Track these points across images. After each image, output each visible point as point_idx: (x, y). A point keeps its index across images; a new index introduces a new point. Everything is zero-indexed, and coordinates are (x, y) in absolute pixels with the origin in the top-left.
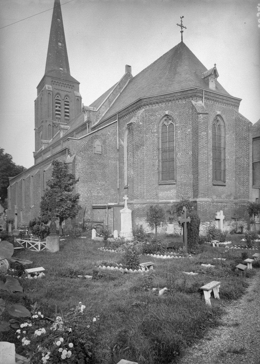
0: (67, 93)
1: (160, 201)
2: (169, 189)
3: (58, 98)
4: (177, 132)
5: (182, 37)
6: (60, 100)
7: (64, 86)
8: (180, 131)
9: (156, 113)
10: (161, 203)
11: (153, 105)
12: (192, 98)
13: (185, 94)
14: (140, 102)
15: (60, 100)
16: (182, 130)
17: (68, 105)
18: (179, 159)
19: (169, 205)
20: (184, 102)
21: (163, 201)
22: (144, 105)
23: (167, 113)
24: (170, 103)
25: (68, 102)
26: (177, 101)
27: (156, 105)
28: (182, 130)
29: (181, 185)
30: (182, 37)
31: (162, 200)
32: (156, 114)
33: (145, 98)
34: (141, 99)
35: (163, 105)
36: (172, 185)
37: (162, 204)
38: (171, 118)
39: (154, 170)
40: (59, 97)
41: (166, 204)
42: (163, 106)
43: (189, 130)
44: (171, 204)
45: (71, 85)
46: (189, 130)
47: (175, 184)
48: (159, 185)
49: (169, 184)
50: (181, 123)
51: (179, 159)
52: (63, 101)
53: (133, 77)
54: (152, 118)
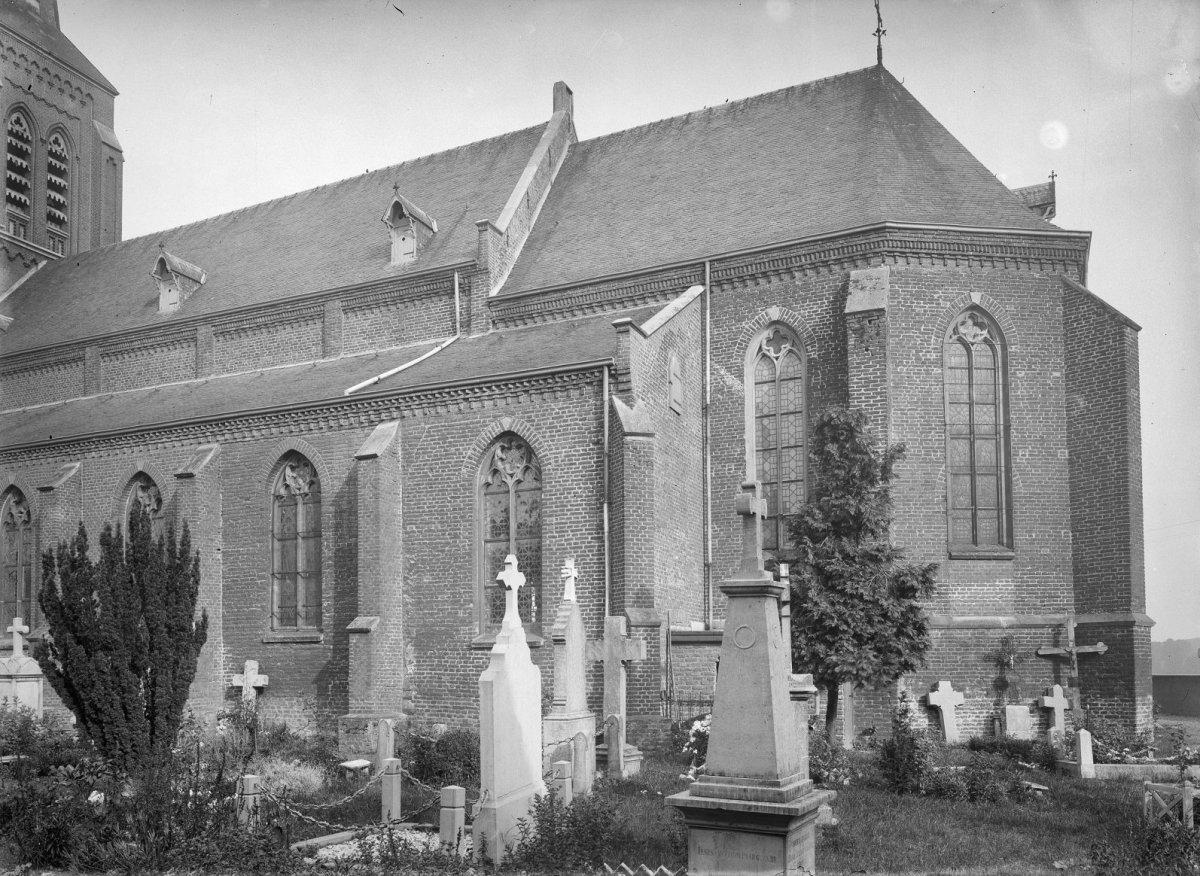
0: (62, 118)
1: (959, 619)
2: (990, 577)
3: (17, 128)
4: (1015, 373)
5: (879, 50)
6: (27, 141)
7: (51, 84)
8: (1023, 373)
9: (935, 293)
10: (961, 627)
11: (924, 261)
12: (917, 260)
13: (1046, 246)
14: (873, 238)
15: (27, 141)
16: (1030, 368)
17: (60, 173)
18: (1023, 473)
19: (991, 633)
20: (1037, 276)
21: (968, 618)
22: (891, 254)
23: (976, 298)
24: (988, 268)
25: (62, 159)
26: (929, 261)
27: (936, 261)
28: (1030, 368)
29: (1032, 561)
30: (879, 50)
31: (963, 614)
32: (936, 296)
33: (899, 229)
34: (885, 228)
35: (962, 269)
36: (1001, 563)
37: (966, 631)
38: (986, 321)
39: (928, 502)
40: (21, 125)
41: (981, 631)
42: (960, 270)
43: (1057, 374)
44: (1000, 631)
45: (78, 89)
46: (1057, 374)
47: (1009, 559)
48: (951, 558)
49: (989, 559)
50: (1029, 345)
51: (1023, 473)
52: (43, 151)
53: (580, 140)
54: (920, 307)
